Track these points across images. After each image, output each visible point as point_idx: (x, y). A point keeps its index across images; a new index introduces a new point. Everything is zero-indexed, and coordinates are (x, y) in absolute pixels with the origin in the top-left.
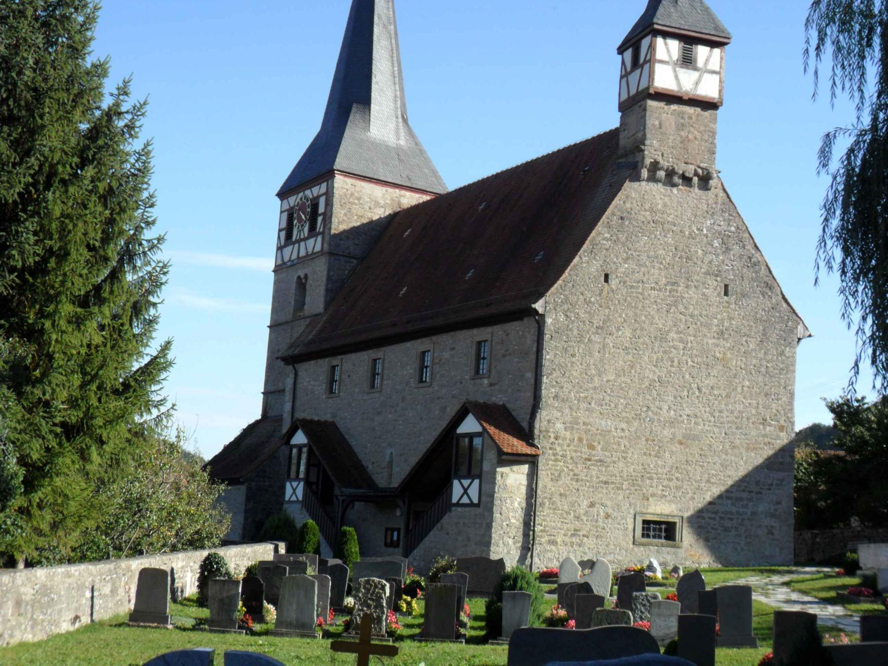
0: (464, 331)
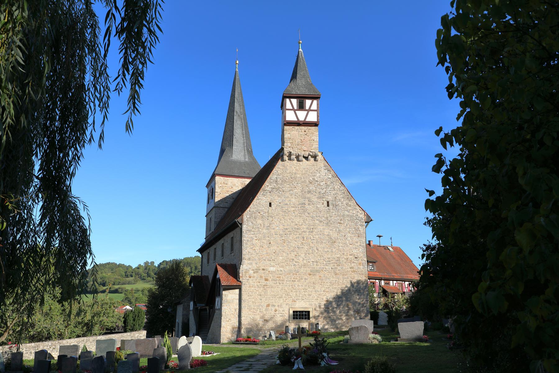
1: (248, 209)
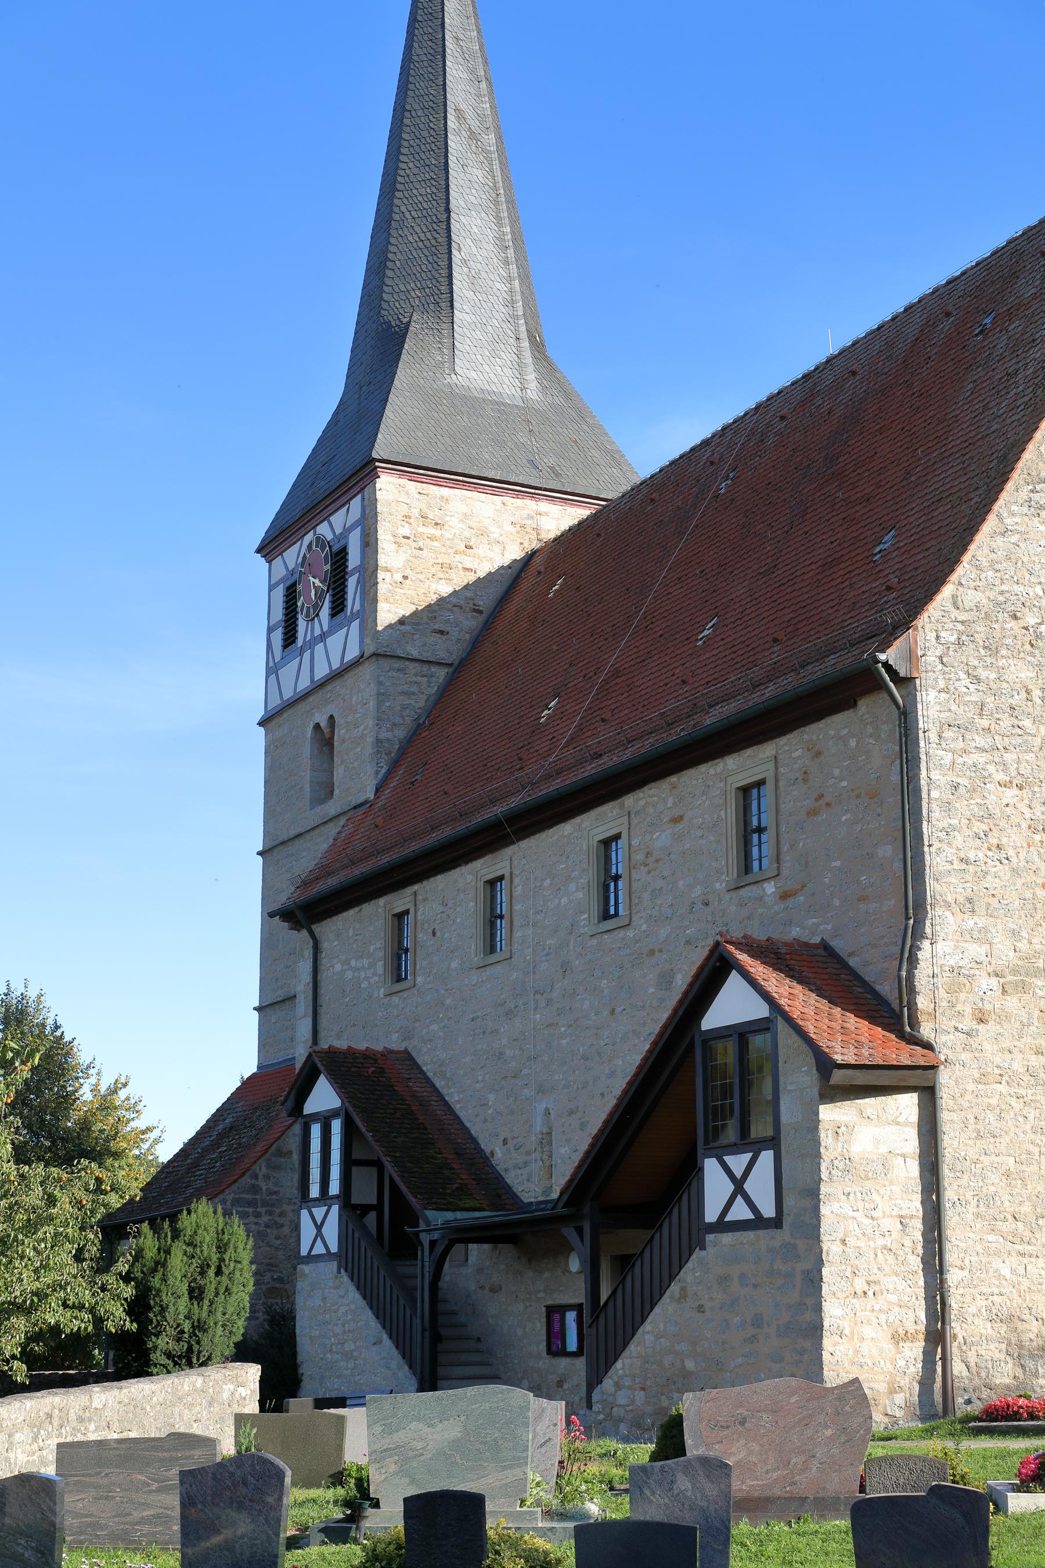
0: (703, 768)
1: (947, 591)
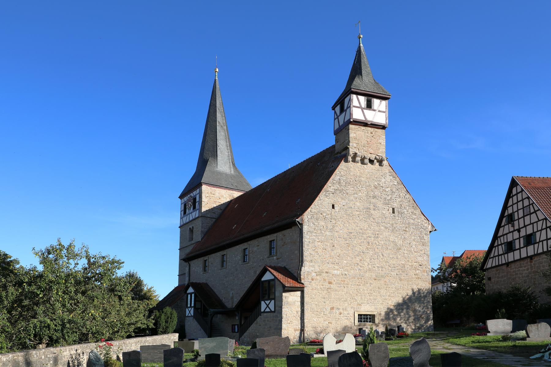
1: (309, 209)
